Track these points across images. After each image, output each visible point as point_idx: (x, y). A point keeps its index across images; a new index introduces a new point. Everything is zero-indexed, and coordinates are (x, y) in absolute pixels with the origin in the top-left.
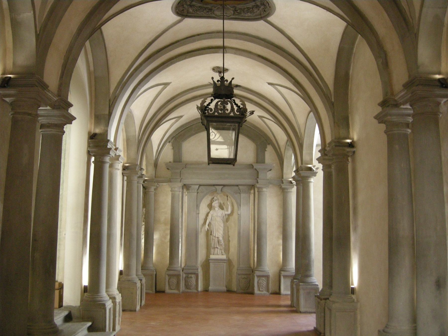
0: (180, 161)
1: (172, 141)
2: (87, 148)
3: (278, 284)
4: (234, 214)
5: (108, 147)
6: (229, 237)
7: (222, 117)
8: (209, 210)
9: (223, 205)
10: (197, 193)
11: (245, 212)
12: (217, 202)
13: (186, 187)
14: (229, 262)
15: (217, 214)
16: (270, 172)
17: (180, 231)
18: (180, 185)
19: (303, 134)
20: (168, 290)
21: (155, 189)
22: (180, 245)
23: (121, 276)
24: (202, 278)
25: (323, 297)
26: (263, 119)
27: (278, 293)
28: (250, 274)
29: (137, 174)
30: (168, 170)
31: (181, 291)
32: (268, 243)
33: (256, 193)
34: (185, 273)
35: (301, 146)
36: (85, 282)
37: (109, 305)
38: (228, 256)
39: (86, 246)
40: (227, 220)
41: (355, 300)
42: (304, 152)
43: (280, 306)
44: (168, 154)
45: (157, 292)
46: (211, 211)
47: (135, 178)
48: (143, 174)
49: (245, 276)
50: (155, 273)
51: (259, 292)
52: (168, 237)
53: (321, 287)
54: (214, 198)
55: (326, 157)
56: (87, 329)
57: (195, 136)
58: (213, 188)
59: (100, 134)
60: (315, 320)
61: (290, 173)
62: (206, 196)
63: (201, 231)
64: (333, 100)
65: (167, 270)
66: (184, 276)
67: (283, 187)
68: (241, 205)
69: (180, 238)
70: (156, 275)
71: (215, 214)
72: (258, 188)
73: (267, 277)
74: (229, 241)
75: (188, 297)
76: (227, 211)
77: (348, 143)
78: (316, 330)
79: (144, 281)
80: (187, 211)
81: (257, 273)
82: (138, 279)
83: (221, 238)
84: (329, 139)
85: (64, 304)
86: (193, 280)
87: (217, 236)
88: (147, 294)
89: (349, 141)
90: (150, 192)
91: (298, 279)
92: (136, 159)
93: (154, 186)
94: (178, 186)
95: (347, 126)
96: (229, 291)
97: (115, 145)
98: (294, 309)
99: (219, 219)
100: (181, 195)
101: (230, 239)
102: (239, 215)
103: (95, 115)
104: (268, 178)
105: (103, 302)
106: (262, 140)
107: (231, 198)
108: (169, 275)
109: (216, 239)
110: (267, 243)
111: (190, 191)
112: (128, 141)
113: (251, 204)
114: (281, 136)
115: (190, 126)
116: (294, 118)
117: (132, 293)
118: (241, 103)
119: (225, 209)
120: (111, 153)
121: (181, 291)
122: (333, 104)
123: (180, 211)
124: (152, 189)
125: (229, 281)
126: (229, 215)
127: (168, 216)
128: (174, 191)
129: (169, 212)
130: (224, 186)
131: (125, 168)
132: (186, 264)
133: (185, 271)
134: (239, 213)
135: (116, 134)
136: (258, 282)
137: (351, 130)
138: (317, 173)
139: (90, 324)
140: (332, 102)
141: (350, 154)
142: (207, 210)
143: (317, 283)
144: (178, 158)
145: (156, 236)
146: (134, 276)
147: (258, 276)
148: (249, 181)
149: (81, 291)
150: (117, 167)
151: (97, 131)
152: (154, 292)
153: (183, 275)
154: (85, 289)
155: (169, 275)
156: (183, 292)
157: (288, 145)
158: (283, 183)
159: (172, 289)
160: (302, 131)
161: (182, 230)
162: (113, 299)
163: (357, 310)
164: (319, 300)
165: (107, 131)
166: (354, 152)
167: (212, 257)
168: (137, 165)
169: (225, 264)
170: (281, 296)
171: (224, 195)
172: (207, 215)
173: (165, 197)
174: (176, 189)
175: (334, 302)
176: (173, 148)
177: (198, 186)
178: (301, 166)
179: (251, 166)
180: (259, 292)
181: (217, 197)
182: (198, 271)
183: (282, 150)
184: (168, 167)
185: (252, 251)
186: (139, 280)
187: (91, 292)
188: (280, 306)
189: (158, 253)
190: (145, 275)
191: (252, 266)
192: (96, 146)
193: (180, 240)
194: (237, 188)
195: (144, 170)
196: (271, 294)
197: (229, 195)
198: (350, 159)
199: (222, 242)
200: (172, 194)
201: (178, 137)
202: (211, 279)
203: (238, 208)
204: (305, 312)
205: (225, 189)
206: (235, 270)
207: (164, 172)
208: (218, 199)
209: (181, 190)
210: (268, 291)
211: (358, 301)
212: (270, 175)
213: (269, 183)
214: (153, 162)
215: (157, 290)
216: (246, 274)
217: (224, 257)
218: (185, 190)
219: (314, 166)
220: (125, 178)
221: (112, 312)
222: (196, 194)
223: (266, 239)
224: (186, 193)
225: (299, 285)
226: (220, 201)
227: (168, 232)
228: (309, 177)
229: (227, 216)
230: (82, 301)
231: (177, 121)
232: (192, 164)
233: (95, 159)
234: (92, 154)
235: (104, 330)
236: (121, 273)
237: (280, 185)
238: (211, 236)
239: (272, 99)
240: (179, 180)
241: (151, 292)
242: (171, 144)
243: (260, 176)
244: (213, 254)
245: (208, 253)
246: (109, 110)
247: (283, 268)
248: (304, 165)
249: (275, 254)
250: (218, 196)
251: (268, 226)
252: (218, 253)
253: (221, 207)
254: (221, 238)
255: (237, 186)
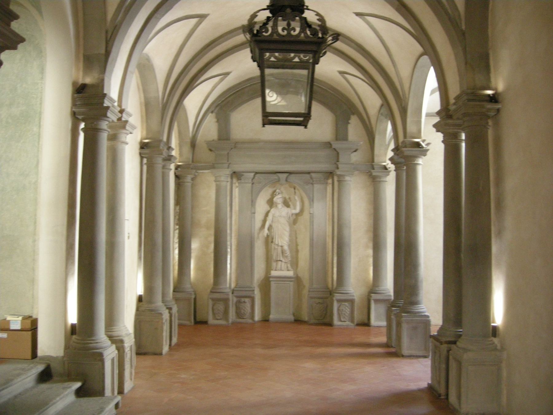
0: (228, 139)
1: (216, 111)
2: (72, 108)
3: (366, 311)
4: (304, 213)
5: (105, 105)
6: (297, 245)
7: (284, 42)
8: (269, 209)
9: (289, 200)
10: (253, 184)
11: (320, 210)
12: (279, 196)
13: (236, 175)
14: (297, 280)
15: (281, 213)
16: (355, 153)
17: (228, 238)
18: (228, 172)
19: (407, 92)
20: (211, 321)
21: (193, 179)
22: (229, 257)
23: (141, 303)
24: (260, 302)
25: (444, 339)
26: (346, 75)
27: (366, 324)
28: (327, 298)
29: (162, 154)
30: (210, 152)
31: (230, 321)
32: (353, 253)
33: (336, 183)
34: (237, 297)
35: (404, 111)
36: (73, 318)
37: (110, 353)
38: (296, 273)
39: (73, 263)
40: (295, 222)
41: (499, 347)
42: (409, 120)
43: (369, 345)
44: (210, 129)
45: (197, 322)
46: (272, 210)
47: (159, 161)
48: (172, 156)
49: (321, 301)
50: (193, 297)
51: (340, 323)
52: (212, 246)
53: (392, 298)
54: (275, 191)
55: (450, 121)
56: (73, 393)
57: (248, 103)
58: (275, 177)
59: (93, 86)
60: (428, 370)
61: (386, 155)
62: (266, 188)
63: (258, 238)
64: (463, 27)
65: (211, 292)
66: (235, 299)
67: (374, 174)
68: (315, 200)
69: (229, 247)
70: (195, 299)
71: (277, 214)
72: (339, 176)
73: (352, 302)
74: (297, 251)
75: (241, 330)
76: (295, 209)
77: (489, 95)
78: (430, 388)
79: (175, 309)
80: (237, 209)
81: (337, 296)
82: (165, 308)
83: (286, 248)
84: (454, 91)
85: (40, 353)
86: (248, 306)
87: (280, 245)
88: (180, 325)
89: (490, 92)
90: (184, 182)
91: (399, 307)
92: (161, 132)
93: (191, 174)
94: (224, 174)
95: (487, 69)
96: (298, 321)
97: (120, 105)
98: (393, 350)
99: (283, 221)
100: (229, 188)
101: (299, 248)
102: (312, 215)
103: (85, 56)
104: (352, 162)
105: (121, 338)
106: (344, 107)
107: (301, 191)
108: (213, 299)
109: (280, 249)
110: (350, 254)
111: (243, 181)
112: (147, 106)
113: (328, 199)
114: (371, 100)
115: (243, 89)
116: (393, 69)
117: (156, 329)
118: (318, 17)
119: (291, 206)
120: (109, 114)
121: (230, 321)
122: (464, 34)
123: (228, 209)
124: (189, 178)
125: (298, 308)
126: (297, 215)
127: (212, 215)
128: (219, 181)
129: (213, 211)
130: (290, 173)
131: (143, 146)
132: (237, 284)
133: (235, 294)
134: (311, 212)
135: (120, 86)
136: (338, 310)
137: (492, 75)
138: (427, 150)
139: (78, 385)
140: (462, 30)
141: (492, 114)
142: (266, 207)
143: (426, 314)
144: (224, 134)
145: (195, 245)
146: (159, 303)
147: (339, 301)
148: (325, 167)
149: (66, 332)
150: (123, 139)
151: (88, 80)
152: (193, 323)
153: (233, 300)
154: (73, 329)
155: (213, 299)
156: (233, 323)
157: (382, 114)
158: (373, 169)
159: (218, 319)
160: (406, 86)
161: (231, 236)
162: (118, 343)
163: (501, 362)
164: (437, 344)
165: (103, 80)
166: (498, 110)
167: (274, 273)
168: (161, 141)
169: (292, 283)
170: (371, 328)
171: (291, 187)
172: (267, 215)
173: (207, 190)
174: (222, 179)
175: (466, 350)
176: (218, 121)
177: (253, 174)
178: (403, 142)
179: (328, 145)
180: (340, 323)
181: (280, 189)
182: (254, 293)
183: (373, 121)
184: (211, 147)
185: (330, 265)
186: (167, 308)
187: (81, 335)
188: (369, 345)
189: (198, 269)
190: (176, 300)
191: (330, 286)
192: (86, 105)
193: (229, 250)
194: (308, 175)
195: (173, 149)
196: (358, 325)
197: (297, 187)
198: (490, 122)
199: (288, 253)
200: (217, 185)
201: (225, 105)
202: (273, 305)
203: (310, 205)
204: (410, 357)
205: (292, 178)
206: (305, 292)
207: (204, 155)
208: (282, 193)
209: (229, 179)
210: (352, 321)
211: (503, 349)
212: (355, 158)
213: (355, 168)
214: (189, 140)
215: (198, 319)
216: (321, 298)
217: (291, 273)
218: (235, 180)
219: (424, 141)
220: (145, 161)
221: (116, 364)
222: (250, 185)
223: (350, 249)
224: (236, 184)
225: (402, 317)
226: (284, 196)
227: (212, 239)
228: (416, 157)
229: (294, 217)
230: (67, 347)
231: (222, 80)
232: (243, 142)
233: (85, 125)
234: (80, 117)
235: (101, 393)
236: (140, 299)
237: (370, 172)
238: (273, 245)
239: (360, 41)
240: (226, 165)
241: (187, 323)
242: (214, 114)
243: (341, 160)
244: (276, 270)
245: (268, 268)
246: (106, 47)
247: (373, 289)
248: (408, 139)
249: (364, 269)
250: (282, 189)
251: (352, 230)
252: (283, 269)
253: (286, 204)
254: (286, 248)
255: (309, 173)
